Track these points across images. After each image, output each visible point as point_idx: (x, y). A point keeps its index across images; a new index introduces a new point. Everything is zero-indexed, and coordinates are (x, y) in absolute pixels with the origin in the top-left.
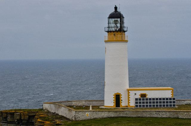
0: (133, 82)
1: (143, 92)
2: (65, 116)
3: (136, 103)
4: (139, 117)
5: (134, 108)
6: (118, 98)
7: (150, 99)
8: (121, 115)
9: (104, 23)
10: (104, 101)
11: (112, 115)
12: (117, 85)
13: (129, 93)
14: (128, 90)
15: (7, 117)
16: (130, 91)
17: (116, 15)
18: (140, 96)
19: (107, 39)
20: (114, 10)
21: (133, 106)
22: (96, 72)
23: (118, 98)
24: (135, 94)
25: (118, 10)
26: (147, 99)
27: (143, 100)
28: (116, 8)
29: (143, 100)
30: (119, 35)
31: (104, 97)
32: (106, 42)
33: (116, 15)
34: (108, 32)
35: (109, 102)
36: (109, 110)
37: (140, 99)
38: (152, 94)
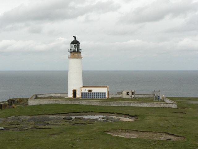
0: (86, 83)
1: (90, 89)
2: (17, 98)
3: (82, 95)
4: (67, 104)
5: (81, 98)
6: (75, 92)
7: (94, 93)
8: (56, 103)
9: (68, 47)
10: (67, 94)
11: (70, 103)
12: (75, 84)
13: (81, 89)
14: (81, 88)
15: (12, 102)
16: (82, 88)
17: (75, 43)
18: (88, 91)
19: (70, 57)
20: (74, 39)
21: (80, 97)
22: (62, 79)
23: (75, 92)
24: (85, 90)
25: (77, 39)
26: (92, 93)
27: (90, 93)
28: (75, 38)
29: (90, 93)
30: (76, 55)
31: (68, 92)
32: (69, 58)
33: (75, 43)
34: (70, 52)
35: (70, 95)
36: (70, 99)
37: (88, 93)
38: (95, 90)
